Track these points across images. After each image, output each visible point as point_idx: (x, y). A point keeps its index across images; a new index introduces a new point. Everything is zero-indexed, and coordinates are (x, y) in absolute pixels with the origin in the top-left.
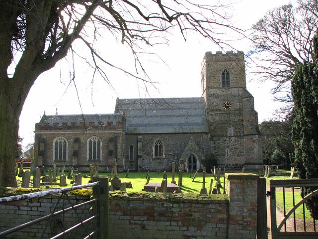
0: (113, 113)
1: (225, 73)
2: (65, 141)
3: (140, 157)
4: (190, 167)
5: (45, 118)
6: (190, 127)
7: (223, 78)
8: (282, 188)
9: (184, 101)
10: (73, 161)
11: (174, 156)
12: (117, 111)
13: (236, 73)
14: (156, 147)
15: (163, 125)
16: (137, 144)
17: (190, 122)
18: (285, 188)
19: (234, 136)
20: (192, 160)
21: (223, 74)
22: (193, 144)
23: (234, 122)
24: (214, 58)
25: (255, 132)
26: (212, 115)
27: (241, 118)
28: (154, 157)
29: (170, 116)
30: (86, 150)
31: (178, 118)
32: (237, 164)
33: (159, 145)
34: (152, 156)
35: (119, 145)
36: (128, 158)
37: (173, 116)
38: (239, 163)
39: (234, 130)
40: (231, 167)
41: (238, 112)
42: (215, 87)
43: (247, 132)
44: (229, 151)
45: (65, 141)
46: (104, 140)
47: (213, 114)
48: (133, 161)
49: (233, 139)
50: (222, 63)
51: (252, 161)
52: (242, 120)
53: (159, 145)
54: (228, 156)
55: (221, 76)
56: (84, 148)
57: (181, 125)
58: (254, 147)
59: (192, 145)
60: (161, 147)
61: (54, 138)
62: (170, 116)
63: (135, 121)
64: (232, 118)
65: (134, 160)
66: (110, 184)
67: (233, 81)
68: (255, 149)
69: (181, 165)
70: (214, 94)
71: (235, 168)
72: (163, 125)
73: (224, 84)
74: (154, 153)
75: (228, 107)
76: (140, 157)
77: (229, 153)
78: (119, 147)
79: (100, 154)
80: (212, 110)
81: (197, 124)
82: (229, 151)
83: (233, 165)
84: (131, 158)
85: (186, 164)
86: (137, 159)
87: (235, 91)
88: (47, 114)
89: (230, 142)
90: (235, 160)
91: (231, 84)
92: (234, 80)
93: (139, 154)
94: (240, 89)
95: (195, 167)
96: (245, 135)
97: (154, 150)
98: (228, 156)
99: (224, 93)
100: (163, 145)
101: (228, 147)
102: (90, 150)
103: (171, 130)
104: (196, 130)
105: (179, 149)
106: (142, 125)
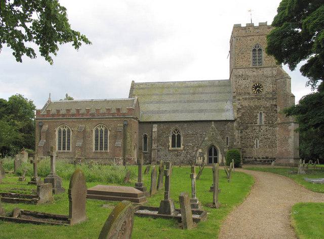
2: (68, 130)
4: (210, 161)
12: (131, 95)
14: (173, 137)
20: (213, 152)
24: (244, 32)
27: (274, 103)
28: (170, 149)
32: (267, 158)
33: (176, 135)
39: (265, 117)
40: (261, 161)
44: (258, 142)
47: (241, 98)
48: (146, 153)
50: (253, 37)
52: (276, 106)
53: (176, 135)
55: (251, 53)
60: (179, 136)
61: (57, 127)
63: (152, 107)
69: (199, 158)
71: (265, 161)
73: (254, 63)
74: (170, 144)
75: (256, 89)
77: (258, 145)
82: (258, 142)
85: (206, 156)
88: (53, 100)
95: (216, 161)
97: (170, 140)
99: (255, 73)
100: (181, 134)
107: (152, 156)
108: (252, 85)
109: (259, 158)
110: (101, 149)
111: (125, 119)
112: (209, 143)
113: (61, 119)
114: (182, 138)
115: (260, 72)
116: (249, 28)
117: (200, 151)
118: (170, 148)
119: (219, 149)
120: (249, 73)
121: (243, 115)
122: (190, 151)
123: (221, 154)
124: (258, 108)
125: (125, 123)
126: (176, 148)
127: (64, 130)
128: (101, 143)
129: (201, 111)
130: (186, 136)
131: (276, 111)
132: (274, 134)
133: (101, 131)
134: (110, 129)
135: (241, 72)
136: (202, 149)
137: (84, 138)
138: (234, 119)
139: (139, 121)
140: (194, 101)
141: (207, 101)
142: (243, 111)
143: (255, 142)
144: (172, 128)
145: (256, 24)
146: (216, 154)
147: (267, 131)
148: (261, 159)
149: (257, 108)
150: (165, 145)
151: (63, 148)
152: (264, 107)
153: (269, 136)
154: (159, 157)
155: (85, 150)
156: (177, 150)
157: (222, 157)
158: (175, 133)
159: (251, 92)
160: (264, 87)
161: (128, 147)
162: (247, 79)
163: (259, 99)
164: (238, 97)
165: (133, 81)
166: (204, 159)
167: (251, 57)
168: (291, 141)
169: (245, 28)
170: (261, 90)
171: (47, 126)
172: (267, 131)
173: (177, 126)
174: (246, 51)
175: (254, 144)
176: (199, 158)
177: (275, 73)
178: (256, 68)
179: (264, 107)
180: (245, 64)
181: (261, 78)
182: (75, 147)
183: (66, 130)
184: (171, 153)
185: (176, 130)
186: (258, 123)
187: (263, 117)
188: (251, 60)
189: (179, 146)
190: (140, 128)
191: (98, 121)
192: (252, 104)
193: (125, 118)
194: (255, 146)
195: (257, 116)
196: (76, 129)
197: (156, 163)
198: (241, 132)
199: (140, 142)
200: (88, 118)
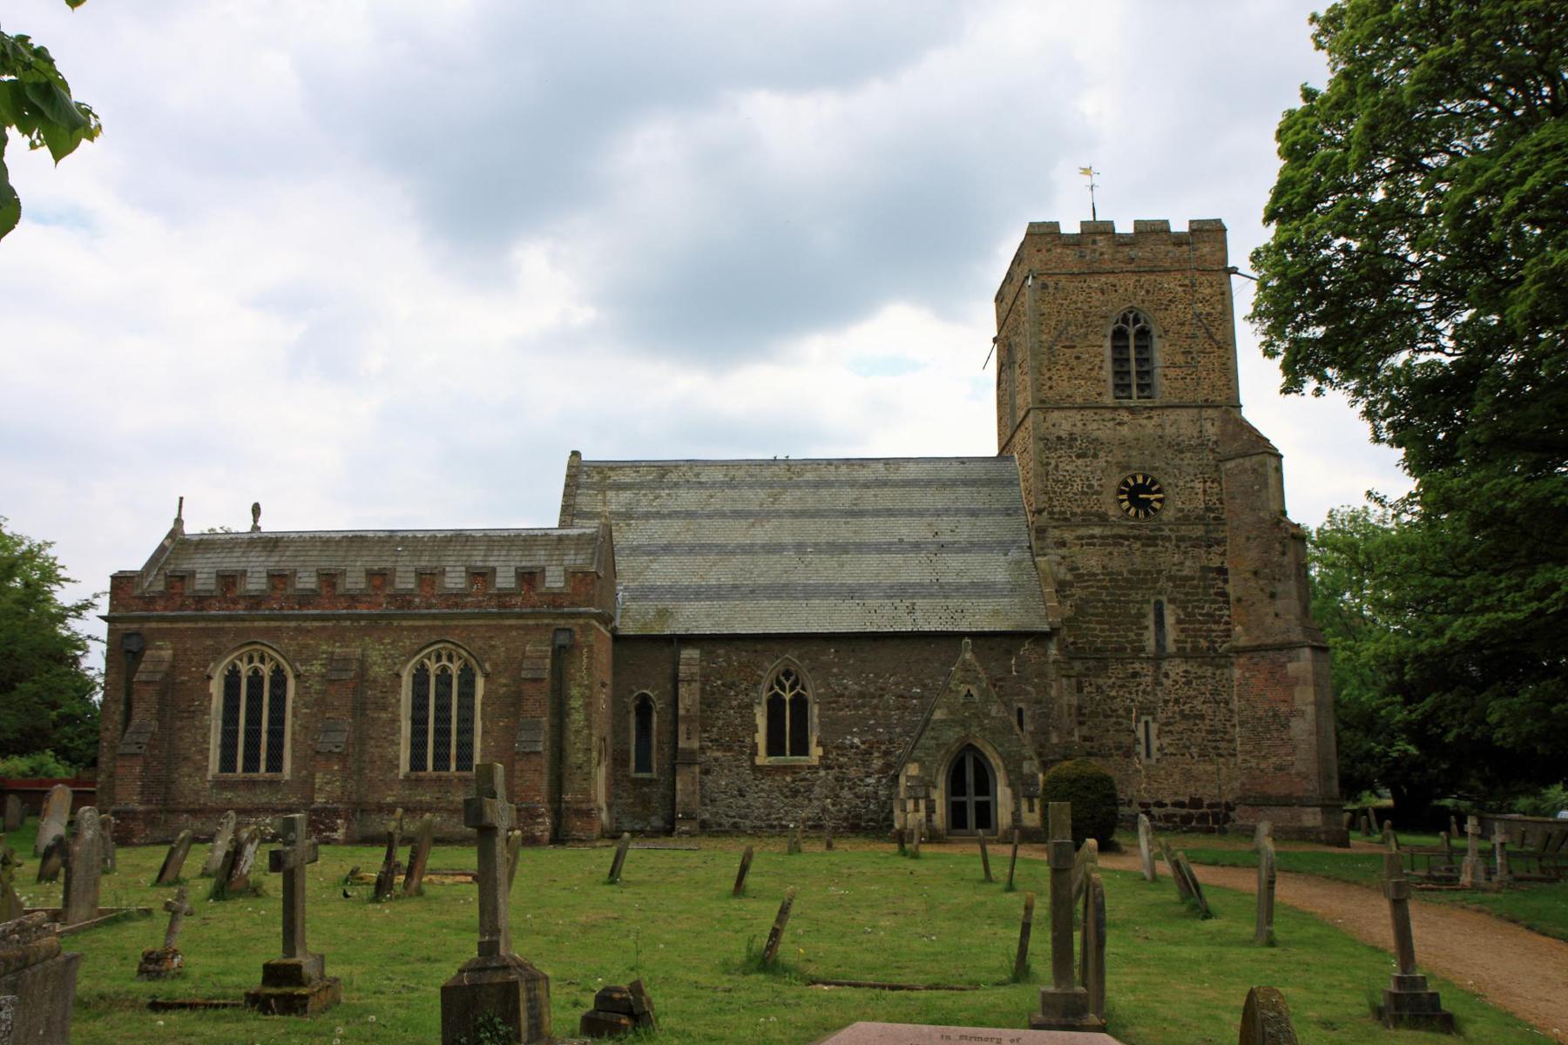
0: (554, 522)
1: (1132, 331)
2: (278, 675)
3: (690, 759)
4: (957, 817)
5: (177, 543)
6: (951, 603)
7: (1120, 360)
8: (976, 849)
9: (911, 472)
10: (319, 779)
11: (868, 752)
12: (569, 511)
13: (1186, 329)
14: (775, 705)
15: (809, 592)
16: (676, 689)
17: (950, 578)
18: (989, 848)
19: (1182, 654)
20: (970, 777)
21: (1119, 335)
22: (974, 691)
23: (1179, 581)
24: (1070, 255)
25: (1296, 635)
26: (1062, 544)
27: (1216, 562)
29: (844, 548)
30: (395, 720)
31: (887, 557)
32: (1196, 803)
33: (788, 696)
34: (754, 753)
35: (575, 692)
36: (626, 763)
37: (860, 548)
38: (1208, 793)
39: (1179, 621)
40: (1168, 818)
41: (1199, 531)
42: (1079, 400)
43: (1247, 630)
44: (1154, 728)
45: (278, 675)
46: (495, 665)
47: (1068, 536)
48: (650, 782)
49: (1176, 669)
50: (1112, 279)
51: (1279, 788)
52: (1222, 571)
53: (788, 696)
54: (1148, 755)
55: (1108, 344)
56: (384, 708)
57: (900, 591)
58: (1292, 714)
59: (969, 694)
60: (800, 704)
61: (218, 654)
62: (844, 548)
63: (664, 572)
64: (1169, 558)
65: (655, 775)
66: (1494, 319)
67: (1172, 373)
68: (1294, 722)
69: (910, 805)
70: (1072, 438)
71: (1186, 820)
72: (809, 592)
73: (1122, 387)
74: (761, 738)
76: (690, 759)
77: (1155, 744)
78: (576, 703)
79: (471, 745)
80: (1064, 520)
81: (983, 589)
82: (1154, 728)
83: (1181, 805)
84: (644, 764)
85: (939, 797)
86: (674, 772)
87: (1181, 424)
88: (191, 528)
89: (1158, 683)
90: (1188, 776)
91: (1163, 386)
92: (1174, 365)
93: (682, 744)
94: (1210, 412)
95: (985, 816)
96: (1240, 651)
97: (761, 721)
98: (1148, 755)
99: (1125, 430)
100: (809, 695)
101: (1147, 709)
102: (419, 722)
103: (847, 619)
104: (981, 617)
105: (895, 715)
106: (698, 593)
107: (678, 799)
108: (1115, 481)
109: (1160, 804)
110: (251, 763)
111: (561, 623)
112: (952, 735)
113: (242, 619)
114: (814, 711)
115: (1149, 425)
116: (1094, 242)
117: (913, 769)
118: (762, 759)
119: (995, 761)
120: (1100, 428)
121: (1080, 609)
122: (852, 772)
123: (1010, 785)
124: (1144, 581)
125: (563, 639)
126: (788, 759)
127: (256, 671)
128: (443, 733)
129: (779, 591)
130: (831, 702)
131: (1224, 594)
132: (1218, 698)
133: (444, 679)
134: (487, 666)
135: (1065, 423)
136: (922, 765)
137: (360, 708)
138: (1046, 628)
139: (614, 631)
140: (860, 548)
141: (917, 546)
142: (1077, 592)
143: (1141, 734)
144: (769, 669)
145: (1124, 227)
146: (984, 784)
147: (1188, 683)
148: (1170, 810)
149: (1142, 579)
150: (737, 744)
151: (436, 757)
152: (1170, 578)
153: (1198, 703)
154: (708, 799)
155: (360, 770)
156: (793, 769)
157: (1016, 797)
158: (783, 688)
159: (1113, 512)
160: (1170, 491)
161: (575, 757)
162: (1095, 456)
163: (1151, 541)
164: (1057, 533)
165: (575, 454)
166: (931, 810)
167: (1108, 366)
168: (1301, 728)
169: (1179, 240)
170: (1157, 505)
171: (167, 654)
172: (1188, 683)
173: (791, 655)
174: (1086, 335)
175: (1137, 741)
176: (910, 805)
177: (1211, 431)
178: (1131, 410)
179: (1170, 578)
180: (1082, 391)
181: (1153, 455)
182: (312, 757)
183: (266, 670)
184: (766, 784)
185: (787, 674)
186: (1150, 643)
187: (1170, 620)
188: (1107, 372)
189: (801, 748)
190: (618, 664)
191: (432, 628)
192: (1116, 564)
193: (562, 615)
194: (1141, 749)
195: (1144, 616)
196: (317, 668)
197: (695, 825)
198: (1080, 689)
199: (618, 729)
200: (381, 617)
